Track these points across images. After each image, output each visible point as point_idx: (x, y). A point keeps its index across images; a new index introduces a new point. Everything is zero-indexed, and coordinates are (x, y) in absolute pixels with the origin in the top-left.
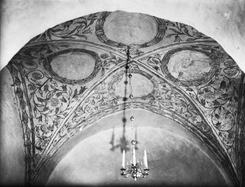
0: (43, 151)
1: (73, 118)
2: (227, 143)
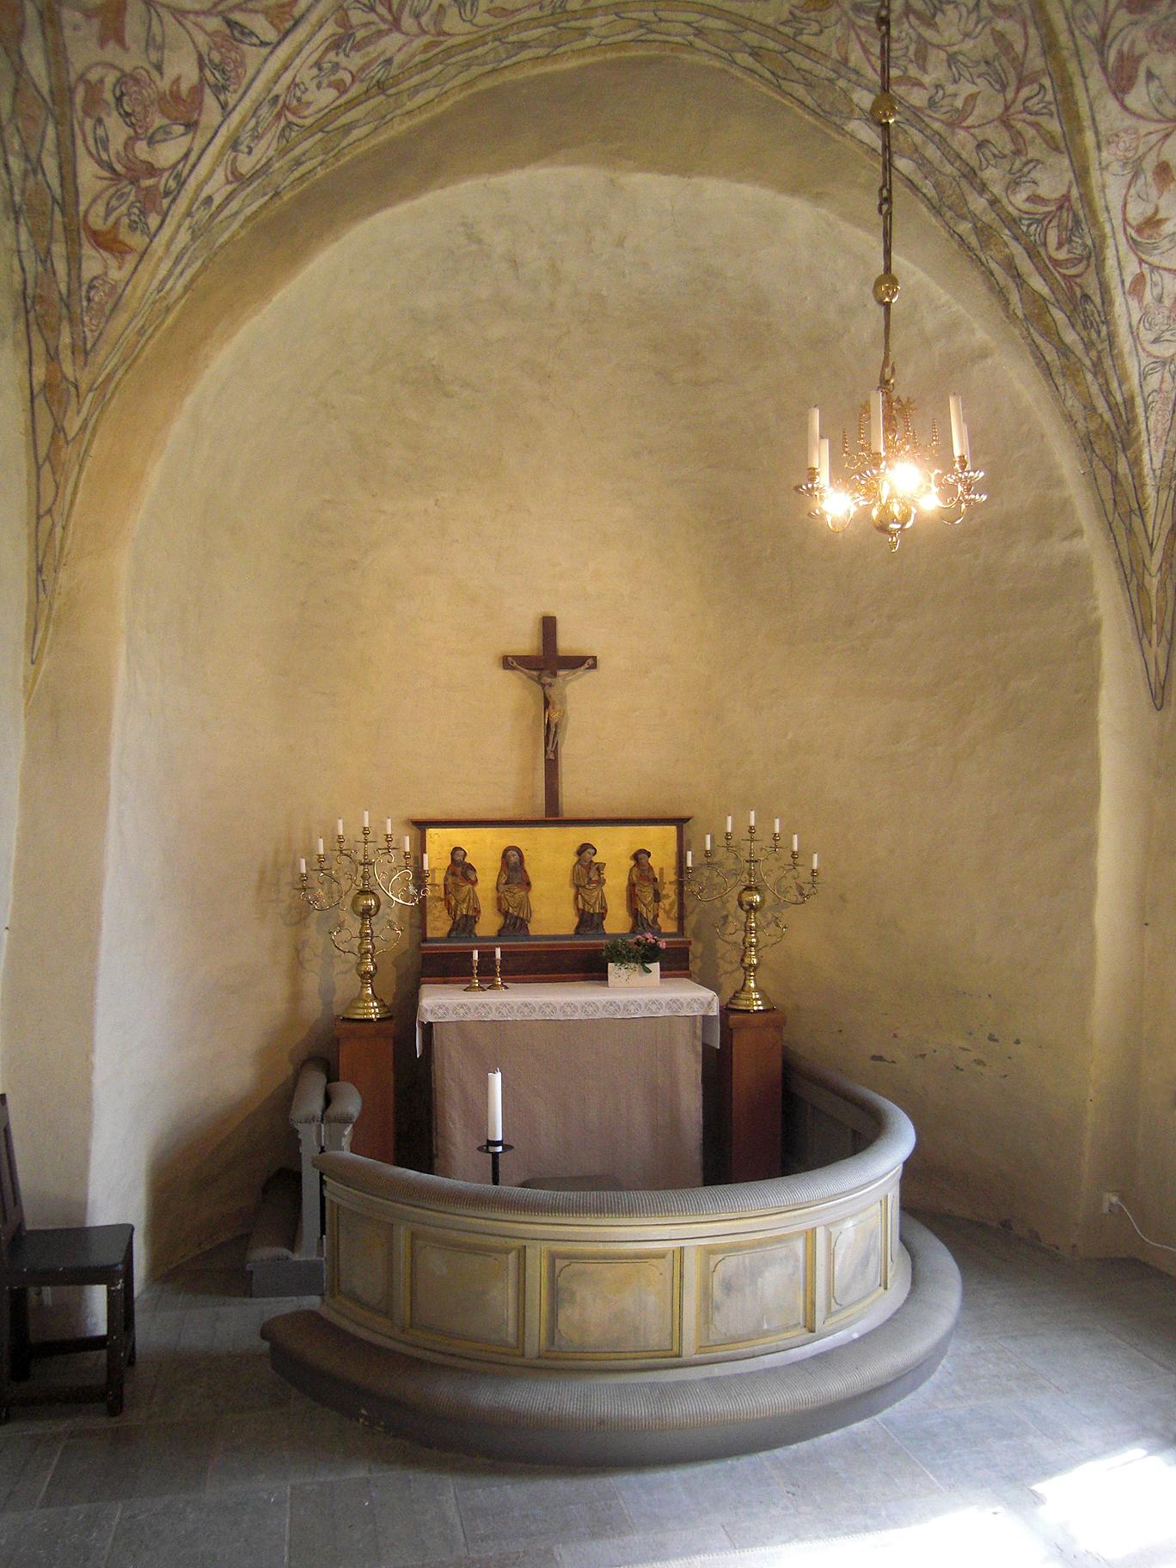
0: (131, 260)
1: (327, 50)
2: (1156, 341)
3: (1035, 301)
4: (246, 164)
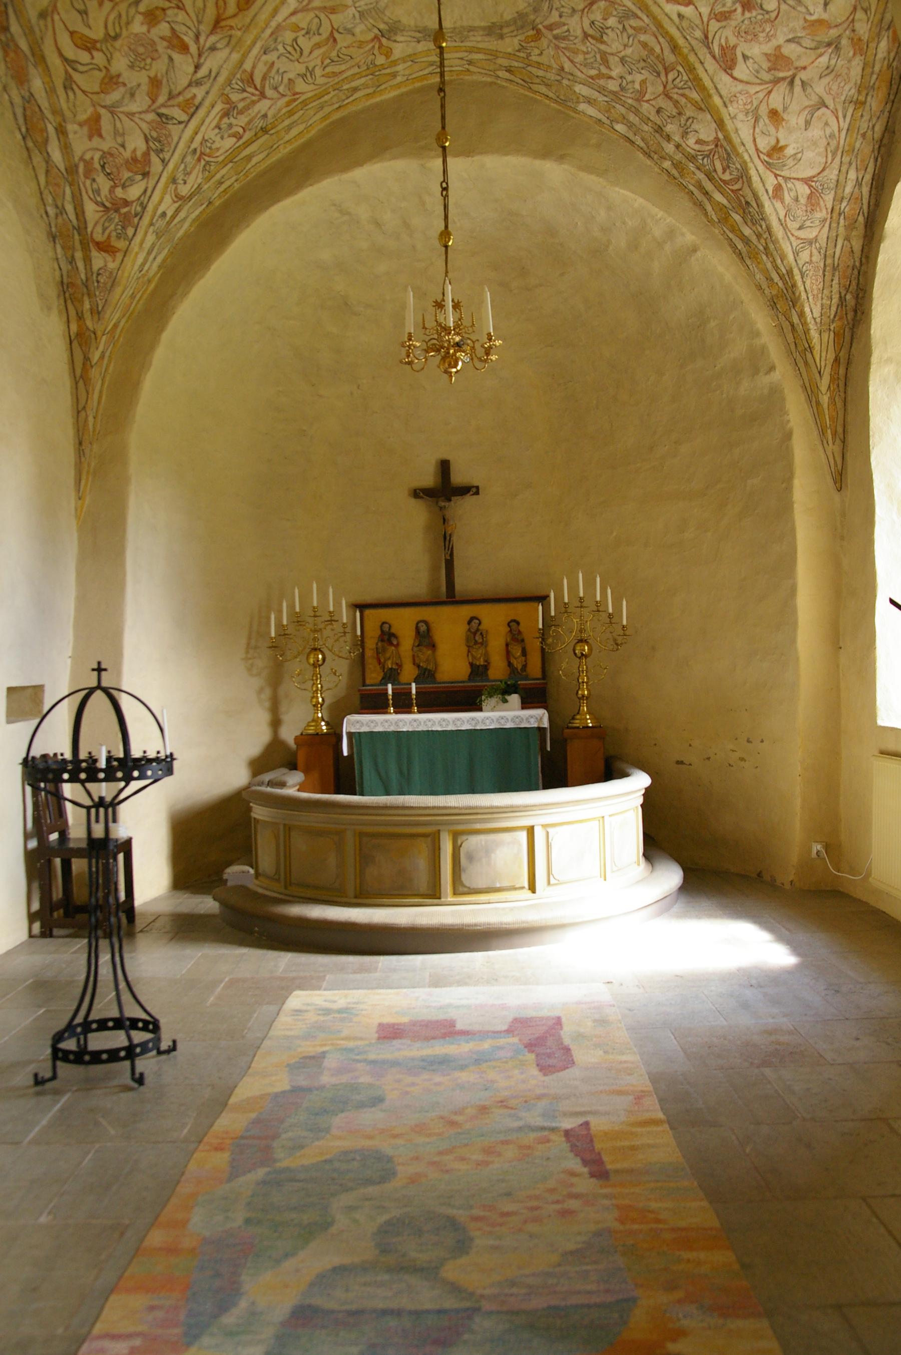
0: (119, 256)
1: (221, 118)
2: (800, 228)
3: (721, 209)
4: (184, 190)
